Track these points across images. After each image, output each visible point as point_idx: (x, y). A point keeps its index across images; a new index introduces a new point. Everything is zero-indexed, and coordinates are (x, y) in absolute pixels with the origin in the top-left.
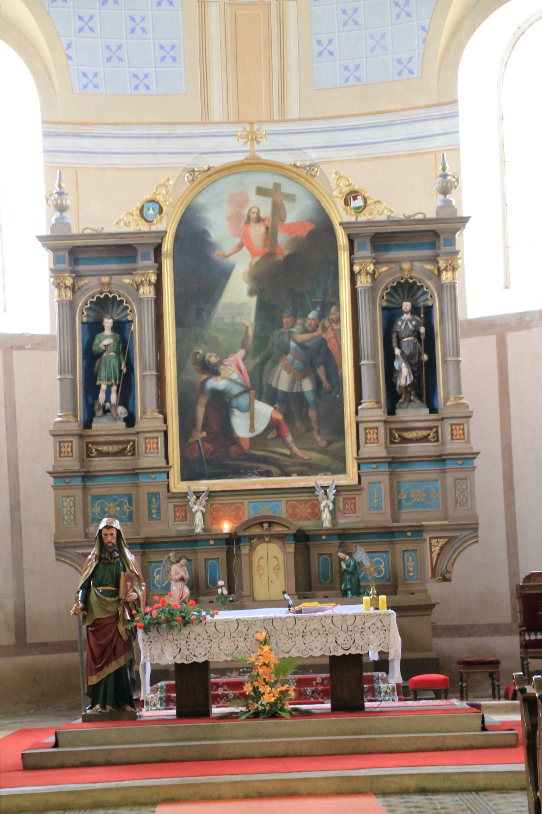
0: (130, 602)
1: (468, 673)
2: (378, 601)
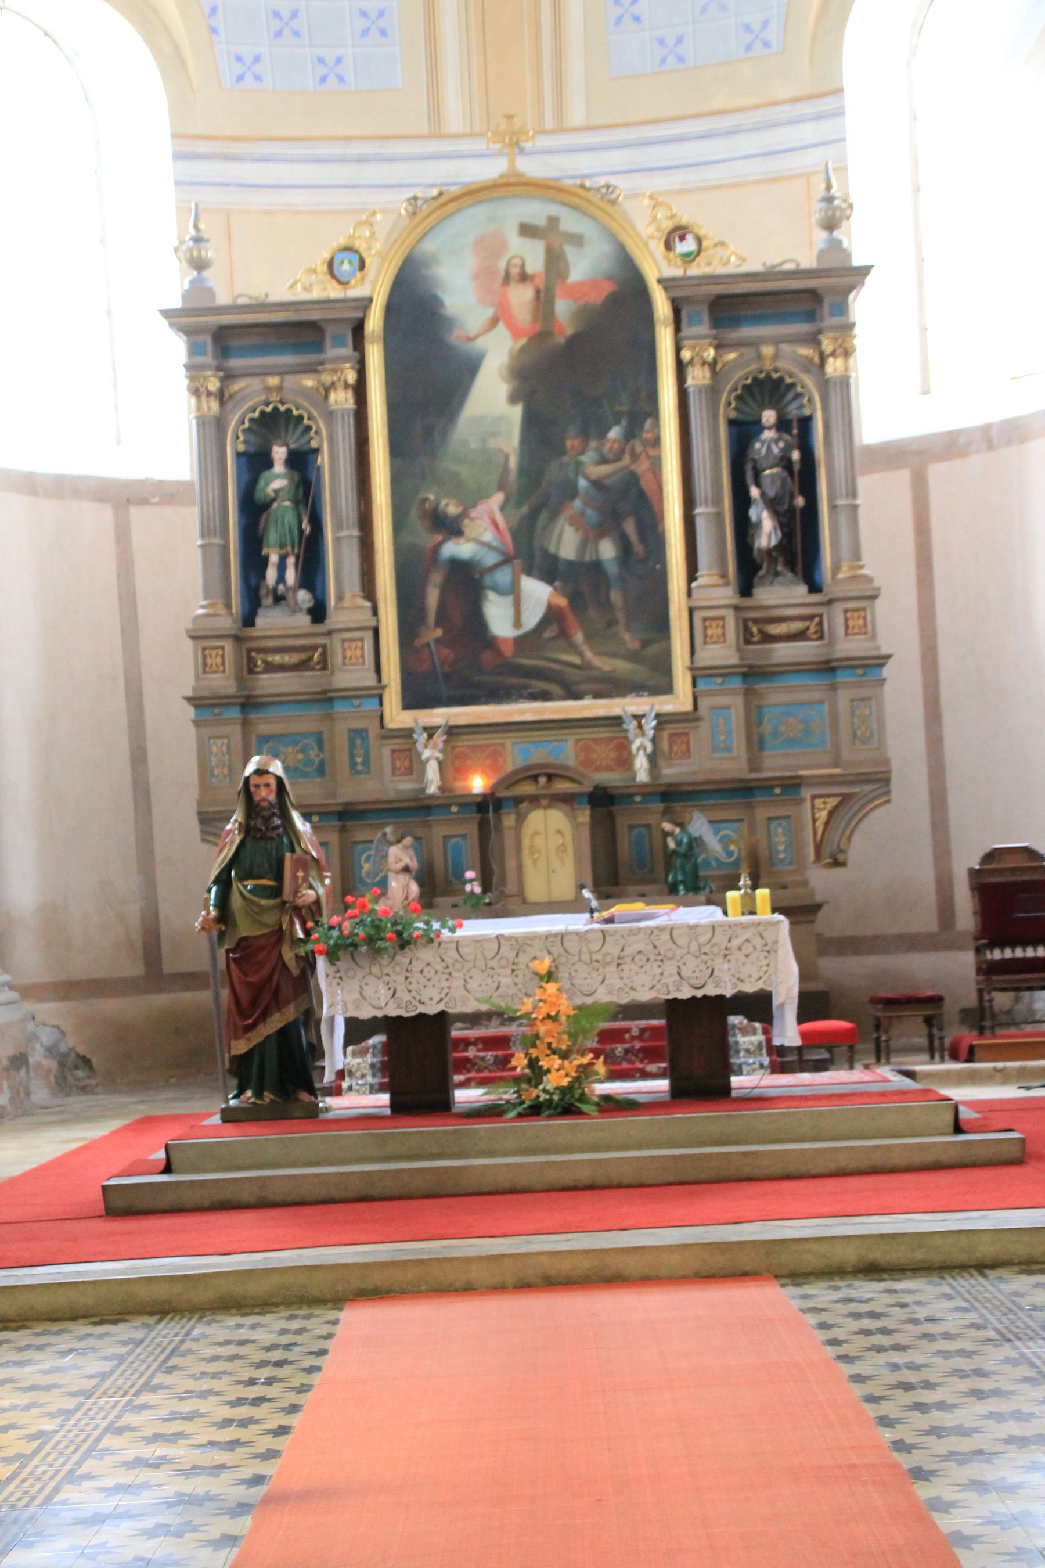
0: (303, 907)
1: (890, 1018)
2: (753, 899)
